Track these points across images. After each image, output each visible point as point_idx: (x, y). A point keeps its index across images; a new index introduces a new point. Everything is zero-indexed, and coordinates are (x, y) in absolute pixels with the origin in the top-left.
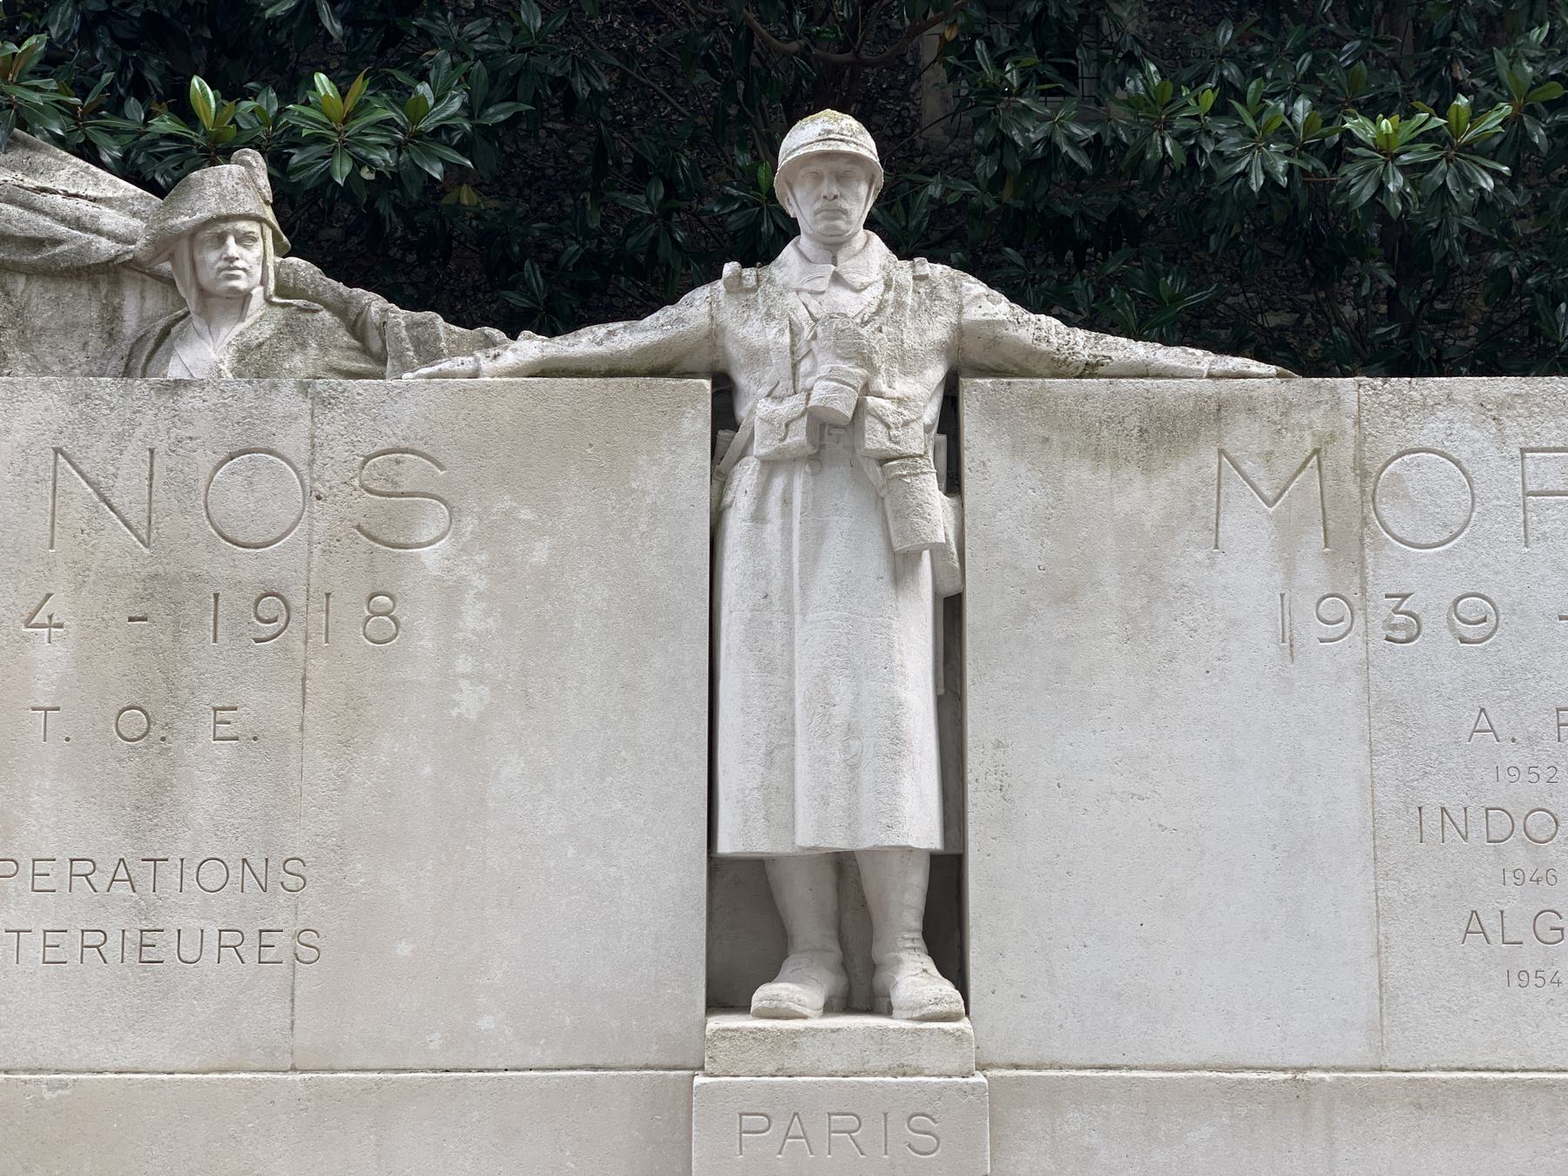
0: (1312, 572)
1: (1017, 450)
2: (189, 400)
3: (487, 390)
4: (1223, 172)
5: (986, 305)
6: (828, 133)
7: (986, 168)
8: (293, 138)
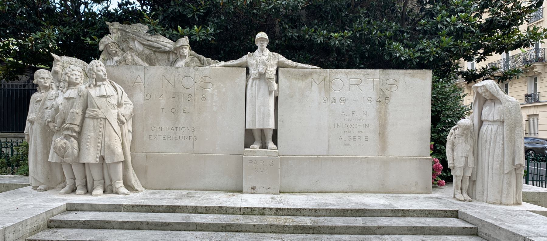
0: (323, 94)
1: (286, 78)
2: (179, 70)
3: (217, 69)
4: (315, 40)
5: (282, 58)
6: (262, 35)
7: (283, 39)
8: (192, 34)
